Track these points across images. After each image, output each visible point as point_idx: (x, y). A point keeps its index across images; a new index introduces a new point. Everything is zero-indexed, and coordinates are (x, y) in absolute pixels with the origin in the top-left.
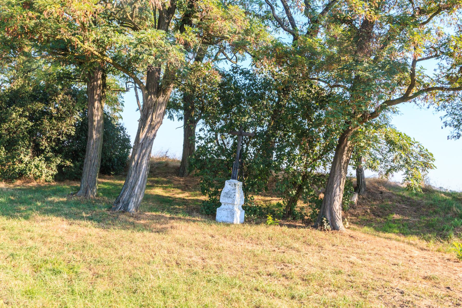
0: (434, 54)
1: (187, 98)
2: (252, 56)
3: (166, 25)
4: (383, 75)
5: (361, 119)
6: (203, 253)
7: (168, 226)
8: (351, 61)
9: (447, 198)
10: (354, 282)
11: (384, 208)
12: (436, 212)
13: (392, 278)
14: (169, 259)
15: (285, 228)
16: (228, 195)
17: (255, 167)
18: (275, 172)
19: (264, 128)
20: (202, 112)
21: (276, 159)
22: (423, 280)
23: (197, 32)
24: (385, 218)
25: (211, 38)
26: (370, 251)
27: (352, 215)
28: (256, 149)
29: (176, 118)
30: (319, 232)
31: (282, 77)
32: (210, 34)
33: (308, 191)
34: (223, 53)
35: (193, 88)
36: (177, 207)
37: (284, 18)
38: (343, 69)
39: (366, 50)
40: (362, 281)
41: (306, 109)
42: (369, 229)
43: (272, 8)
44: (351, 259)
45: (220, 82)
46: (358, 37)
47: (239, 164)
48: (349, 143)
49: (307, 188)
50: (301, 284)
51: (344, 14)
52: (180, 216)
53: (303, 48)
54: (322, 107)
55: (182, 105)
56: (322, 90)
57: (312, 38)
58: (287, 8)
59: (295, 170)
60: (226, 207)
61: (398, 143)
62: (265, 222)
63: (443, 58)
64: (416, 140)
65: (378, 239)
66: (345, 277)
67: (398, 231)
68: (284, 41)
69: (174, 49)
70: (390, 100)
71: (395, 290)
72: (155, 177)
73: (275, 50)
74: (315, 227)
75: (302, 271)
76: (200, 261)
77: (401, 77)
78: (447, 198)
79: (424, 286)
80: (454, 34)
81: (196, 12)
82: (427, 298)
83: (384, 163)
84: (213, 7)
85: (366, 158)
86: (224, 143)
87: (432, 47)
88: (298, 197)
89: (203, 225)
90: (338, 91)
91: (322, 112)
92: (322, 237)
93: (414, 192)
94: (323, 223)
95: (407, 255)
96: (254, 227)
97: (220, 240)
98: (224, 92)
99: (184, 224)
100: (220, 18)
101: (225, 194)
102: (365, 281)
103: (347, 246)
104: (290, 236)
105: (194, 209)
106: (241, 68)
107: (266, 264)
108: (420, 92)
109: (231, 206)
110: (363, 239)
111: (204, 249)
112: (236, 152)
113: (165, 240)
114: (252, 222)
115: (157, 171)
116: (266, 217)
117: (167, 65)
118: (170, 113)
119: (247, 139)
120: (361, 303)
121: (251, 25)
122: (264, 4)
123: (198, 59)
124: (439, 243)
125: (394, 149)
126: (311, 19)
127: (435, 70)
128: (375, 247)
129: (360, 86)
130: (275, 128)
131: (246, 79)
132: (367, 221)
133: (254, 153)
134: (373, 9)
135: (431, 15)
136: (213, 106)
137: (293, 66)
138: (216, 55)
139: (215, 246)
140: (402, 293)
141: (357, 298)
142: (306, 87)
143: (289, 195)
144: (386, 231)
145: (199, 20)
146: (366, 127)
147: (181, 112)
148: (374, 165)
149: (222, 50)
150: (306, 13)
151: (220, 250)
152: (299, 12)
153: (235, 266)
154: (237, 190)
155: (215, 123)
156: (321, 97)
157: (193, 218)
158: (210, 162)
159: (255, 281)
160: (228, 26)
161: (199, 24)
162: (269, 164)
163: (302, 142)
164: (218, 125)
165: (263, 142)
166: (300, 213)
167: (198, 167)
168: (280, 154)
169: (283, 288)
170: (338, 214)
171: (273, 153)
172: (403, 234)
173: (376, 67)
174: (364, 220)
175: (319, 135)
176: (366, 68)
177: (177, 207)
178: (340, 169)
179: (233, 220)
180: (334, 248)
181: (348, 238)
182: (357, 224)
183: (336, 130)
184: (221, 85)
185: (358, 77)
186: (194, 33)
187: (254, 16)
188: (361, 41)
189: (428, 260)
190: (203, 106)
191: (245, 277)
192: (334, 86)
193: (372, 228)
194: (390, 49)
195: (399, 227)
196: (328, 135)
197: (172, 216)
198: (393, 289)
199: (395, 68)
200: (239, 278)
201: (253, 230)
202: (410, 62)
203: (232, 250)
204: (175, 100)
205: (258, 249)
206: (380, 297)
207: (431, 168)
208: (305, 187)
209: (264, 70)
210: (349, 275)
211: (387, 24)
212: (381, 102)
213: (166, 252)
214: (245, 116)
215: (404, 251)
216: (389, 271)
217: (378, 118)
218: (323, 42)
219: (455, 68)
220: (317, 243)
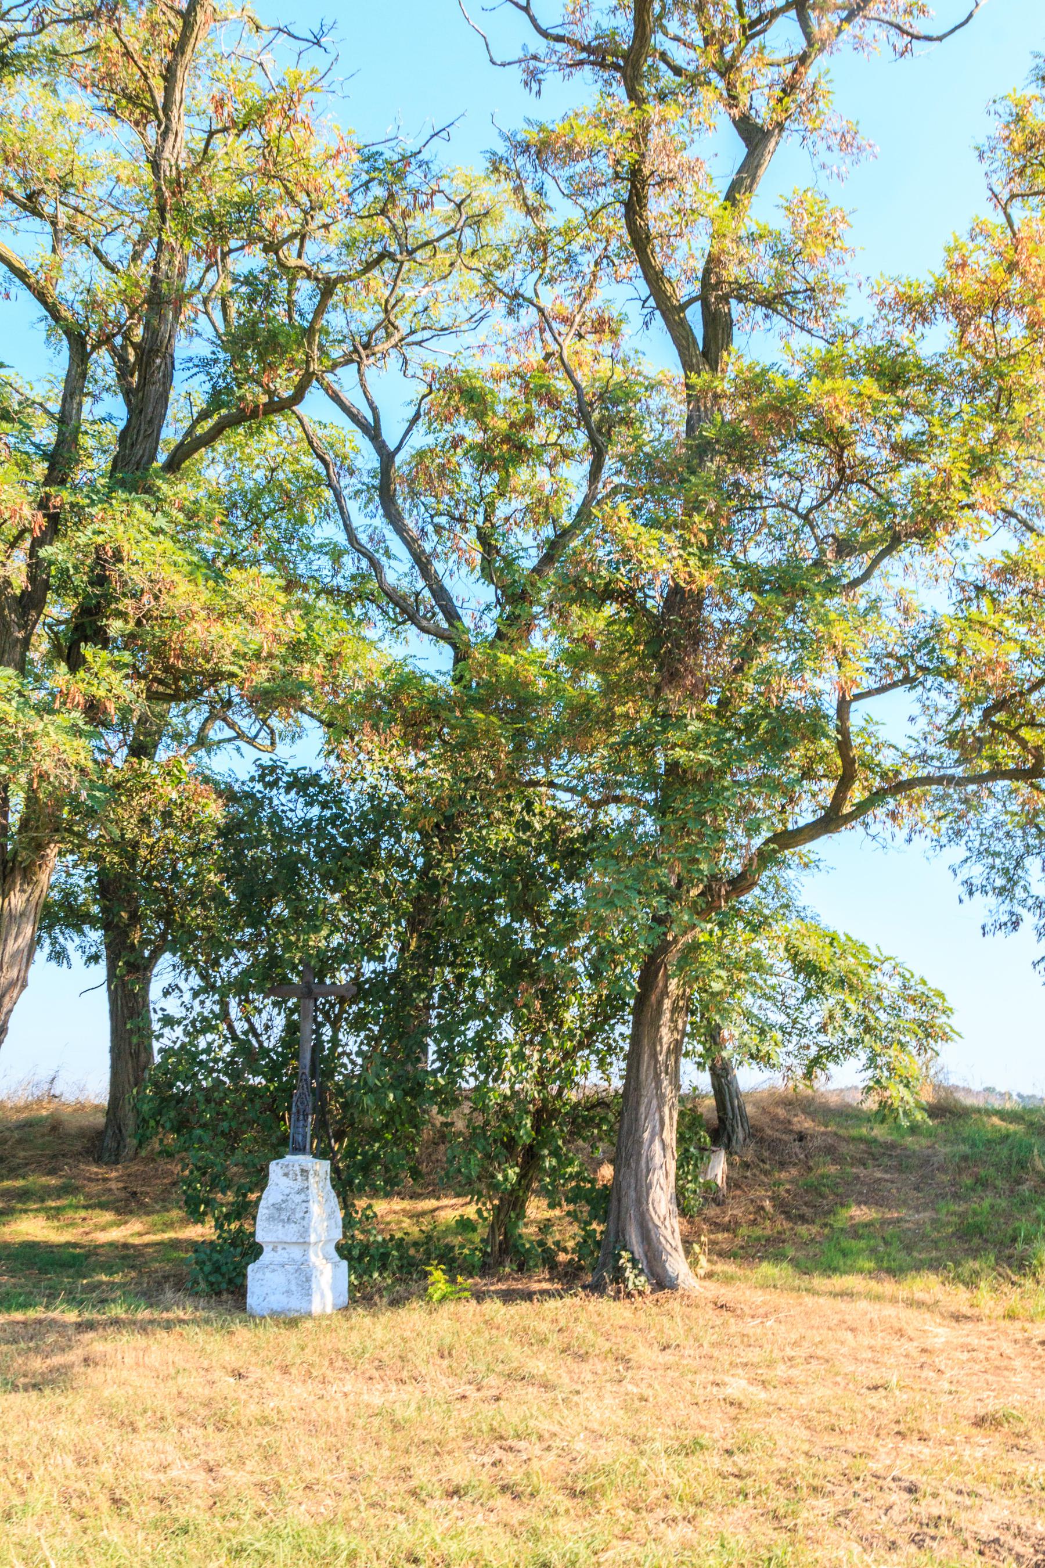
0: (899, 675)
1: (108, 887)
2: (321, 722)
3: (18, 649)
4: (755, 750)
5: (701, 903)
6: (207, 1445)
7: (74, 1357)
8: (646, 715)
9: (1012, 1127)
10: (749, 1474)
11: (814, 1189)
12: (983, 1183)
13: (873, 1439)
14: (85, 1487)
15: (493, 1307)
16: (282, 1213)
17: (367, 1101)
18: (440, 1112)
19: (387, 964)
20: (169, 924)
21: (437, 1065)
22: (974, 1431)
23: (126, 665)
24: (825, 1225)
25: (176, 680)
26: (789, 1352)
27: (717, 1226)
28: (367, 1037)
29: (77, 958)
30: (612, 1303)
31: (428, 785)
32: (173, 666)
33: (559, 1162)
34: (224, 720)
35: (127, 849)
36: (104, 1278)
37: (417, 594)
38: (625, 744)
39: (689, 681)
40: (774, 1468)
41: (520, 883)
42: (776, 1270)
43: (374, 564)
44: (729, 1391)
45: (221, 821)
46: (656, 641)
47: (310, 1099)
48: (673, 984)
49: (555, 1153)
50: (567, 1511)
51: (603, 573)
52: (118, 1311)
53: (488, 685)
54: (572, 875)
55: (95, 909)
56: (565, 815)
57: (513, 653)
58: (422, 562)
59: (505, 1097)
60: (281, 1256)
61: (831, 968)
62: (423, 1294)
63: (928, 685)
64: (886, 953)
65: (809, 1300)
66: (716, 1461)
67: (872, 1265)
68: (423, 666)
69: (51, 729)
70: (785, 832)
71: (888, 1483)
72: (16, 1178)
73: (397, 699)
74: (597, 1288)
75: (566, 1461)
76: (201, 1477)
77: (810, 753)
78: (1012, 1127)
79: (979, 1453)
80: (951, 610)
81: (117, 600)
82: (995, 1496)
83: (795, 1039)
84: (176, 577)
85: (734, 1032)
86: (252, 1029)
87: (890, 655)
88: (528, 1187)
89: (201, 1337)
90: (617, 814)
91: (575, 890)
92: (622, 1323)
93: (905, 1123)
94: (621, 1270)
95: (912, 1347)
96: (387, 1317)
97: (269, 1385)
98: (239, 855)
99: (133, 1344)
100: (203, 614)
101: (272, 1210)
102: (783, 1464)
103: (713, 1345)
104: (515, 1333)
105: (166, 1278)
106: (288, 769)
107: (437, 1453)
108: (876, 798)
109: (296, 1253)
110: (761, 1311)
111: (211, 1429)
112: (296, 1056)
113: (63, 1417)
114: (376, 1298)
115: (22, 1154)
116: (426, 1275)
117: (30, 782)
118: (54, 942)
119: (332, 1006)
120: (779, 1553)
121: (310, 627)
122: (347, 552)
123: (140, 750)
124: (1006, 1288)
125: (820, 988)
126: (504, 589)
127: (912, 719)
128: (803, 1331)
129: (681, 793)
130: (426, 958)
131: (309, 804)
132: (768, 1240)
133: (360, 1053)
134: (694, 550)
135: (872, 553)
136: (203, 904)
137: (463, 746)
138: (202, 729)
139: (253, 1410)
140: (911, 1490)
141: (764, 1531)
142: (511, 813)
143: (495, 1186)
144: (835, 1270)
145: (132, 623)
146: (721, 925)
147: (95, 935)
148: (764, 1048)
149: (221, 709)
150: (488, 572)
151: (267, 1423)
152: (465, 569)
153: (329, 1478)
154: (314, 1189)
155: (216, 963)
156: (564, 842)
157: (165, 1315)
158: (208, 1101)
159: (403, 1527)
160: (228, 637)
161: (132, 636)
162: (414, 1087)
163: (520, 1000)
164: (229, 968)
165: (387, 1013)
166: (541, 1243)
167: (168, 1125)
168: (451, 1048)
169: (508, 1538)
170: (668, 1233)
171: (424, 1048)
172: (889, 1271)
173: (726, 730)
174: (758, 1239)
175: (573, 970)
176: (697, 738)
177: (104, 1278)
178: (657, 1076)
179: (310, 1302)
180: (668, 1357)
181: (710, 1313)
182: (735, 1256)
183: (626, 945)
184: (226, 832)
185: (673, 767)
186: (116, 666)
187: (318, 595)
188: (670, 651)
189: (982, 1356)
190: (171, 907)
191: (367, 1514)
192: (605, 801)
193: (785, 1265)
194: (764, 670)
195: (873, 1251)
196: (602, 966)
197: (87, 1315)
198: (880, 1482)
199: (782, 730)
200: (347, 1521)
201: (382, 1328)
202: (830, 705)
203: (314, 1415)
204: (68, 895)
205: (403, 1401)
206: (842, 1520)
207: (946, 1038)
208: (546, 1152)
209: (369, 766)
210: (729, 1452)
211: (743, 592)
212: (757, 842)
213: (69, 1461)
214: (317, 929)
215: (900, 1333)
216: (859, 1416)
217: (757, 891)
218: (551, 659)
219: (970, 714)
220: (607, 1345)
